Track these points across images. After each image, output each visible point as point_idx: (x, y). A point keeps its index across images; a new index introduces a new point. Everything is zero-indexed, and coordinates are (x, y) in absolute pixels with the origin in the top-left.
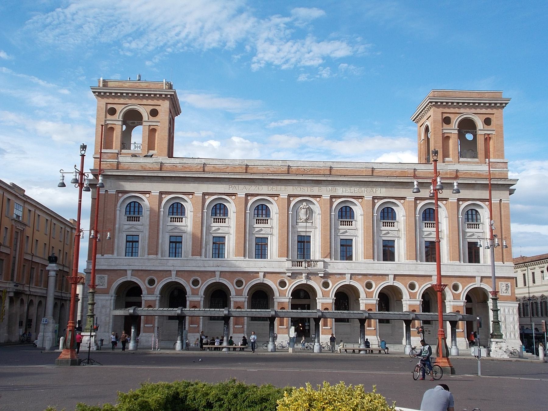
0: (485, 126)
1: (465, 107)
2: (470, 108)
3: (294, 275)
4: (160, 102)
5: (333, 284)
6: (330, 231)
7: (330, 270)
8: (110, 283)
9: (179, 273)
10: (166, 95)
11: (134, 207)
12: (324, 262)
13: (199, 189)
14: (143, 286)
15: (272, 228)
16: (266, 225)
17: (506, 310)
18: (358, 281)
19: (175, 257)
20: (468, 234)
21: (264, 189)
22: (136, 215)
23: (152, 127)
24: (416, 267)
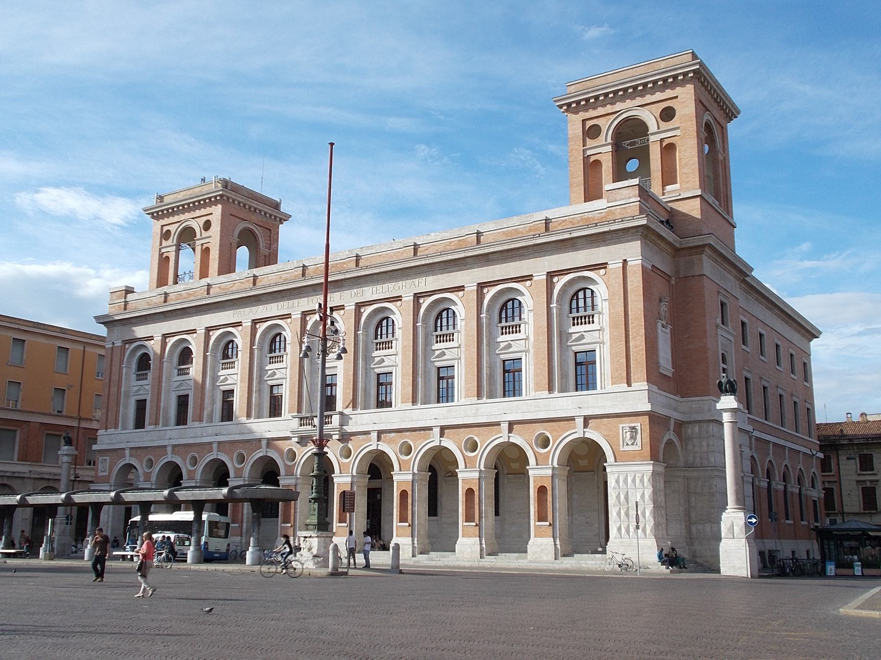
0: (661, 123)
1: (623, 99)
2: (632, 97)
4: (678, 91)
7: (348, 429)
9: (176, 449)
11: (585, 298)
18: (389, 442)
19: (514, 396)
20: (574, 336)
22: (589, 312)
24: (477, 410)
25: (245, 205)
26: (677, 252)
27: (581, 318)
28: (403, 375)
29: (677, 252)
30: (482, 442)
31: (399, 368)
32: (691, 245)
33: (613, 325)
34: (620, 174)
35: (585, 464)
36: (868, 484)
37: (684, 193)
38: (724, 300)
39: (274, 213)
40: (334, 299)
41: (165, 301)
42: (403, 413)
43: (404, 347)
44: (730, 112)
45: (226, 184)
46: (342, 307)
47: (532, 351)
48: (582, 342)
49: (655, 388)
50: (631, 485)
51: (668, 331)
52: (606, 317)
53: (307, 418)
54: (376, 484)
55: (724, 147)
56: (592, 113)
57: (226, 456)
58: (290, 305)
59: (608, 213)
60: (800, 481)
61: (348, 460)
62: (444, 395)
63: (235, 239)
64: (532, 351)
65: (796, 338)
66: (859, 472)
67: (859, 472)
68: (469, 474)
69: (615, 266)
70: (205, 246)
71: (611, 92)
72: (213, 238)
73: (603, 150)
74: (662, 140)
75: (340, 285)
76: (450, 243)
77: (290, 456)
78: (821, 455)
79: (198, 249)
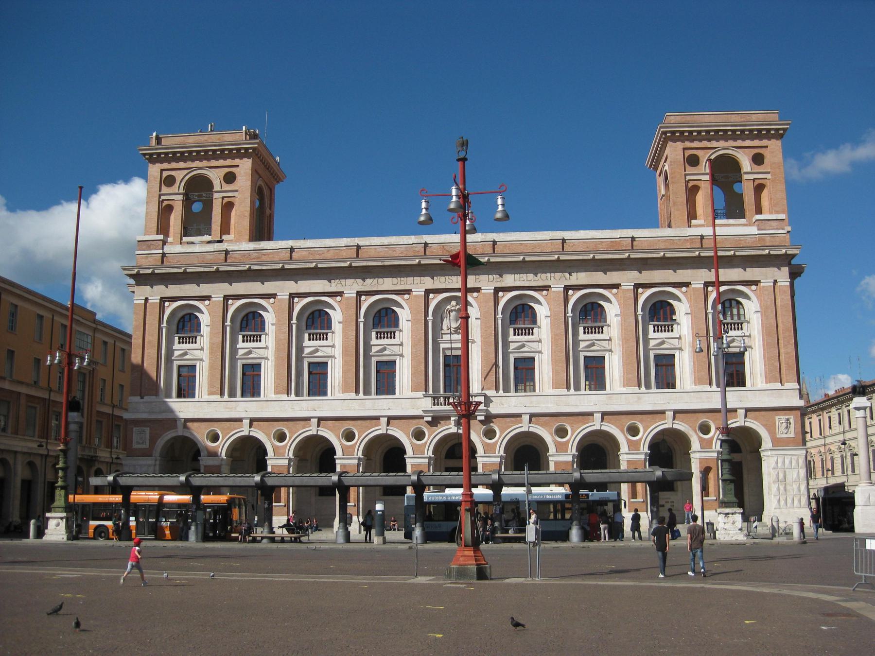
1: (177, 160)
3: (436, 421)
4: (237, 161)
5: (502, 432)
6: (498, 344)
7: (494, 409)
8: (153, 441)
10: (247, 149)
12: (485, 396)
13: (284, 288)
14: (548, 437)
15: (401, 345)
16: (392, 341)
17: (787, 462)
19: (525, 391)
21: (387, 283)
23: (226, 200)
24: (639, 399)
46: (477, 290)
48: (522, 350)
56: (696, 144)
57: (333, 435)
58: (416, 282)
74: (223, 198)
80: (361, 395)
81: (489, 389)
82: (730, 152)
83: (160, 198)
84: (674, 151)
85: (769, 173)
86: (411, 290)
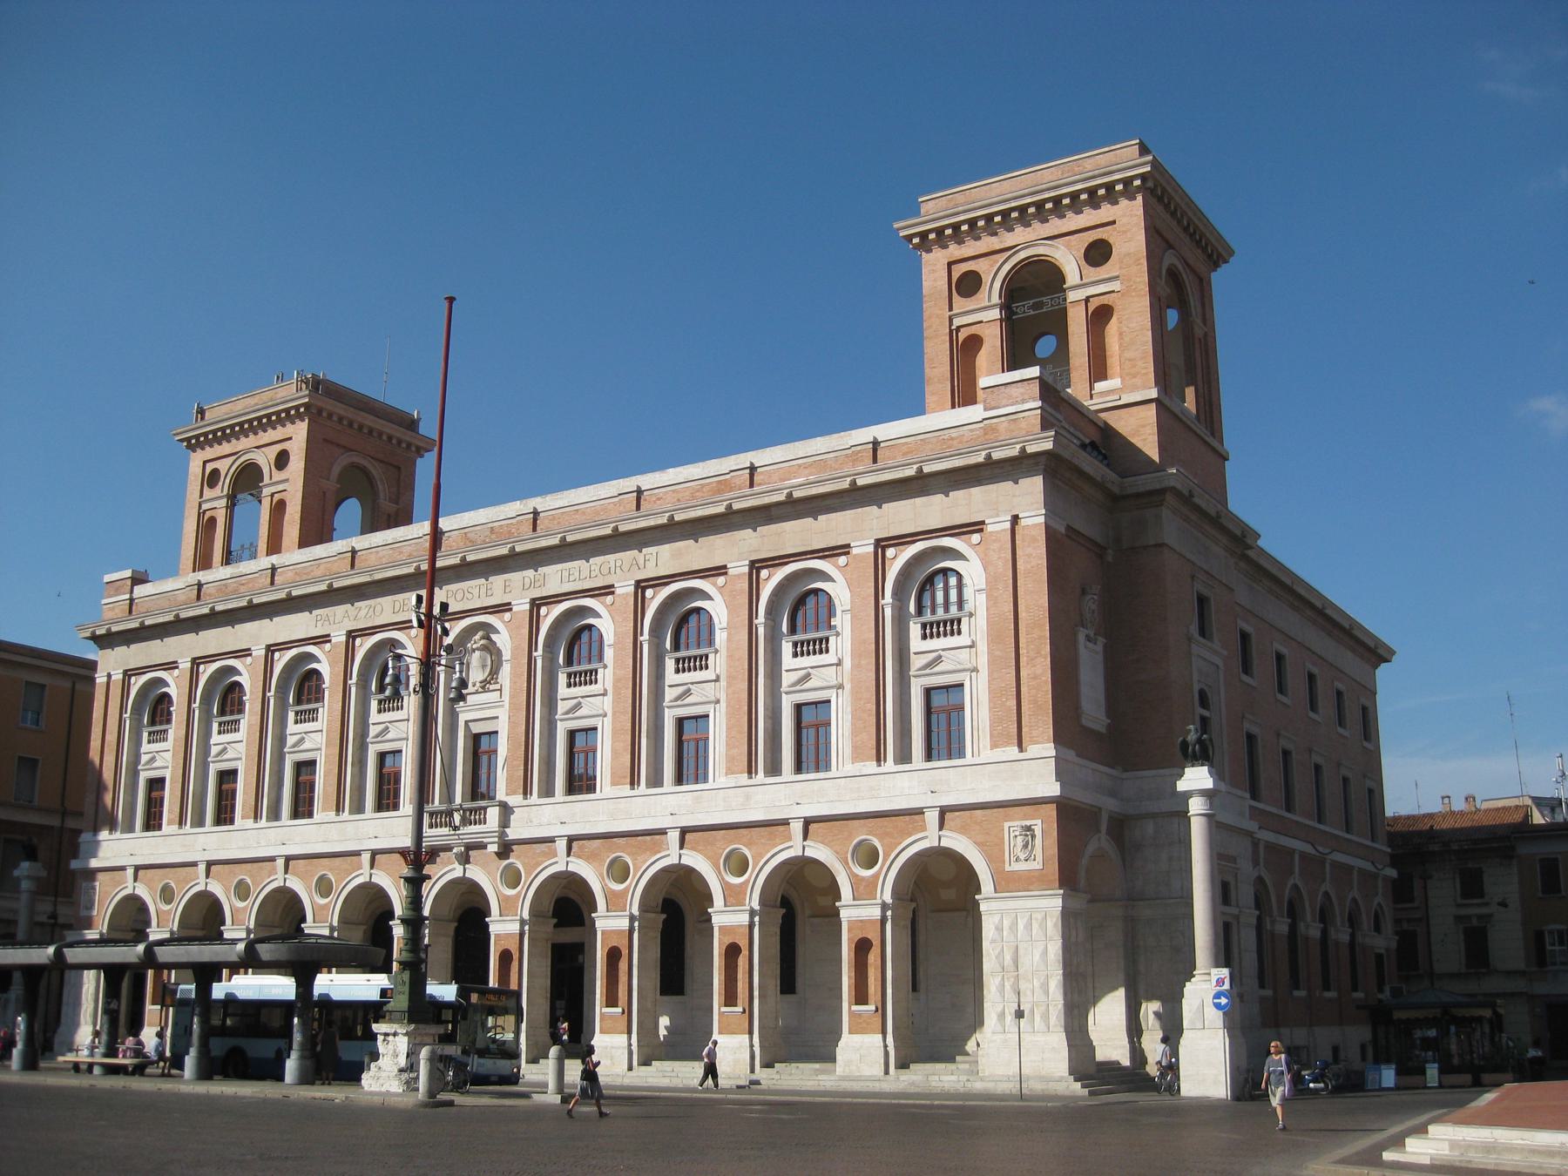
4: (1106, 212)
7: (513, 833)
18: (590, 858)
24: (748, 797)
25: (351, 425)
26: (1115, 501)
27: (932, 625)
28: (615, 733)
29: (1115, 501)
30: (757, 858)
31: (608, 721)
32: (1142, 489)
33: (994, 638)
34: (1015, 358)
35: (939, 900)
36: (1475, 922)
37: (1124, 392)
38: (1205, 592)
39: (407, 436)
40: (451, 595)
41: (199, 597)
42: (613, 806)
43: (617, 681)
44: (1216, 254)
45: (316, 385)
47: (848, 686)
49: (1070, 755)
50: (1023, 935)
51: (1099, 647)
52: (981, 620)
53: (441, 812)
54: (569, 935)
55: (1204, 315)
57: (700, 857)
59: (986, 431)
60: (1353, 921)
61: (622, 886)
62: (690, 768)
63: (331, 485)
64: (848, 686)
65: (1349, 662)
66: (1460, 901)
67: (1460, 901)
68: (732, 916)
69: (998, 526)
70: (277, 497)
71: (997, 214)
72: (290, 484)
73: (984, 314)
74: (1087, 300)
75: (466, 570)
76: (703, 486)
77: (734, 861)
78: (1392, 873)
79: (266, 502)
80: (890, 764)
81: (514, 793)
82: (1040, 250)
83: (951, 323)
84: (934, 265)
85: (1116, 278)
86: (725, 567)
